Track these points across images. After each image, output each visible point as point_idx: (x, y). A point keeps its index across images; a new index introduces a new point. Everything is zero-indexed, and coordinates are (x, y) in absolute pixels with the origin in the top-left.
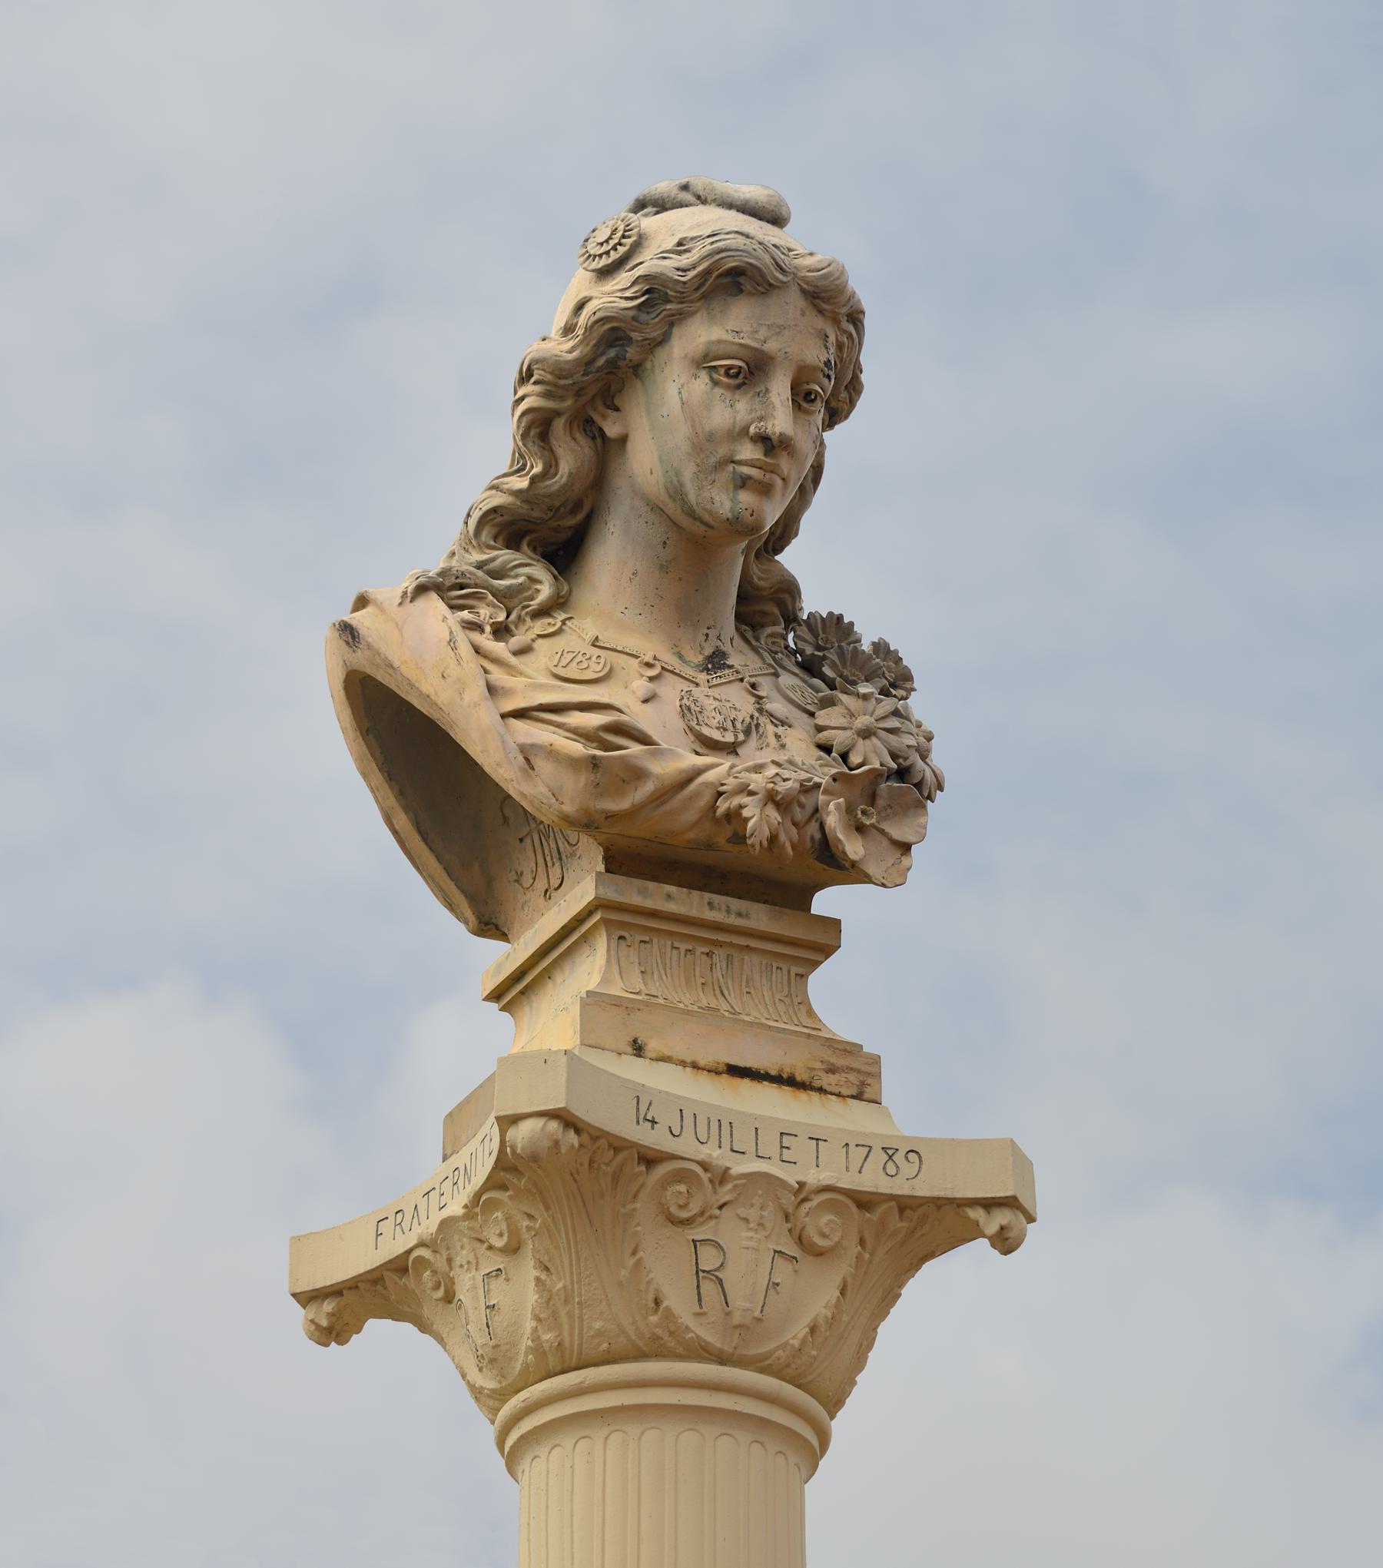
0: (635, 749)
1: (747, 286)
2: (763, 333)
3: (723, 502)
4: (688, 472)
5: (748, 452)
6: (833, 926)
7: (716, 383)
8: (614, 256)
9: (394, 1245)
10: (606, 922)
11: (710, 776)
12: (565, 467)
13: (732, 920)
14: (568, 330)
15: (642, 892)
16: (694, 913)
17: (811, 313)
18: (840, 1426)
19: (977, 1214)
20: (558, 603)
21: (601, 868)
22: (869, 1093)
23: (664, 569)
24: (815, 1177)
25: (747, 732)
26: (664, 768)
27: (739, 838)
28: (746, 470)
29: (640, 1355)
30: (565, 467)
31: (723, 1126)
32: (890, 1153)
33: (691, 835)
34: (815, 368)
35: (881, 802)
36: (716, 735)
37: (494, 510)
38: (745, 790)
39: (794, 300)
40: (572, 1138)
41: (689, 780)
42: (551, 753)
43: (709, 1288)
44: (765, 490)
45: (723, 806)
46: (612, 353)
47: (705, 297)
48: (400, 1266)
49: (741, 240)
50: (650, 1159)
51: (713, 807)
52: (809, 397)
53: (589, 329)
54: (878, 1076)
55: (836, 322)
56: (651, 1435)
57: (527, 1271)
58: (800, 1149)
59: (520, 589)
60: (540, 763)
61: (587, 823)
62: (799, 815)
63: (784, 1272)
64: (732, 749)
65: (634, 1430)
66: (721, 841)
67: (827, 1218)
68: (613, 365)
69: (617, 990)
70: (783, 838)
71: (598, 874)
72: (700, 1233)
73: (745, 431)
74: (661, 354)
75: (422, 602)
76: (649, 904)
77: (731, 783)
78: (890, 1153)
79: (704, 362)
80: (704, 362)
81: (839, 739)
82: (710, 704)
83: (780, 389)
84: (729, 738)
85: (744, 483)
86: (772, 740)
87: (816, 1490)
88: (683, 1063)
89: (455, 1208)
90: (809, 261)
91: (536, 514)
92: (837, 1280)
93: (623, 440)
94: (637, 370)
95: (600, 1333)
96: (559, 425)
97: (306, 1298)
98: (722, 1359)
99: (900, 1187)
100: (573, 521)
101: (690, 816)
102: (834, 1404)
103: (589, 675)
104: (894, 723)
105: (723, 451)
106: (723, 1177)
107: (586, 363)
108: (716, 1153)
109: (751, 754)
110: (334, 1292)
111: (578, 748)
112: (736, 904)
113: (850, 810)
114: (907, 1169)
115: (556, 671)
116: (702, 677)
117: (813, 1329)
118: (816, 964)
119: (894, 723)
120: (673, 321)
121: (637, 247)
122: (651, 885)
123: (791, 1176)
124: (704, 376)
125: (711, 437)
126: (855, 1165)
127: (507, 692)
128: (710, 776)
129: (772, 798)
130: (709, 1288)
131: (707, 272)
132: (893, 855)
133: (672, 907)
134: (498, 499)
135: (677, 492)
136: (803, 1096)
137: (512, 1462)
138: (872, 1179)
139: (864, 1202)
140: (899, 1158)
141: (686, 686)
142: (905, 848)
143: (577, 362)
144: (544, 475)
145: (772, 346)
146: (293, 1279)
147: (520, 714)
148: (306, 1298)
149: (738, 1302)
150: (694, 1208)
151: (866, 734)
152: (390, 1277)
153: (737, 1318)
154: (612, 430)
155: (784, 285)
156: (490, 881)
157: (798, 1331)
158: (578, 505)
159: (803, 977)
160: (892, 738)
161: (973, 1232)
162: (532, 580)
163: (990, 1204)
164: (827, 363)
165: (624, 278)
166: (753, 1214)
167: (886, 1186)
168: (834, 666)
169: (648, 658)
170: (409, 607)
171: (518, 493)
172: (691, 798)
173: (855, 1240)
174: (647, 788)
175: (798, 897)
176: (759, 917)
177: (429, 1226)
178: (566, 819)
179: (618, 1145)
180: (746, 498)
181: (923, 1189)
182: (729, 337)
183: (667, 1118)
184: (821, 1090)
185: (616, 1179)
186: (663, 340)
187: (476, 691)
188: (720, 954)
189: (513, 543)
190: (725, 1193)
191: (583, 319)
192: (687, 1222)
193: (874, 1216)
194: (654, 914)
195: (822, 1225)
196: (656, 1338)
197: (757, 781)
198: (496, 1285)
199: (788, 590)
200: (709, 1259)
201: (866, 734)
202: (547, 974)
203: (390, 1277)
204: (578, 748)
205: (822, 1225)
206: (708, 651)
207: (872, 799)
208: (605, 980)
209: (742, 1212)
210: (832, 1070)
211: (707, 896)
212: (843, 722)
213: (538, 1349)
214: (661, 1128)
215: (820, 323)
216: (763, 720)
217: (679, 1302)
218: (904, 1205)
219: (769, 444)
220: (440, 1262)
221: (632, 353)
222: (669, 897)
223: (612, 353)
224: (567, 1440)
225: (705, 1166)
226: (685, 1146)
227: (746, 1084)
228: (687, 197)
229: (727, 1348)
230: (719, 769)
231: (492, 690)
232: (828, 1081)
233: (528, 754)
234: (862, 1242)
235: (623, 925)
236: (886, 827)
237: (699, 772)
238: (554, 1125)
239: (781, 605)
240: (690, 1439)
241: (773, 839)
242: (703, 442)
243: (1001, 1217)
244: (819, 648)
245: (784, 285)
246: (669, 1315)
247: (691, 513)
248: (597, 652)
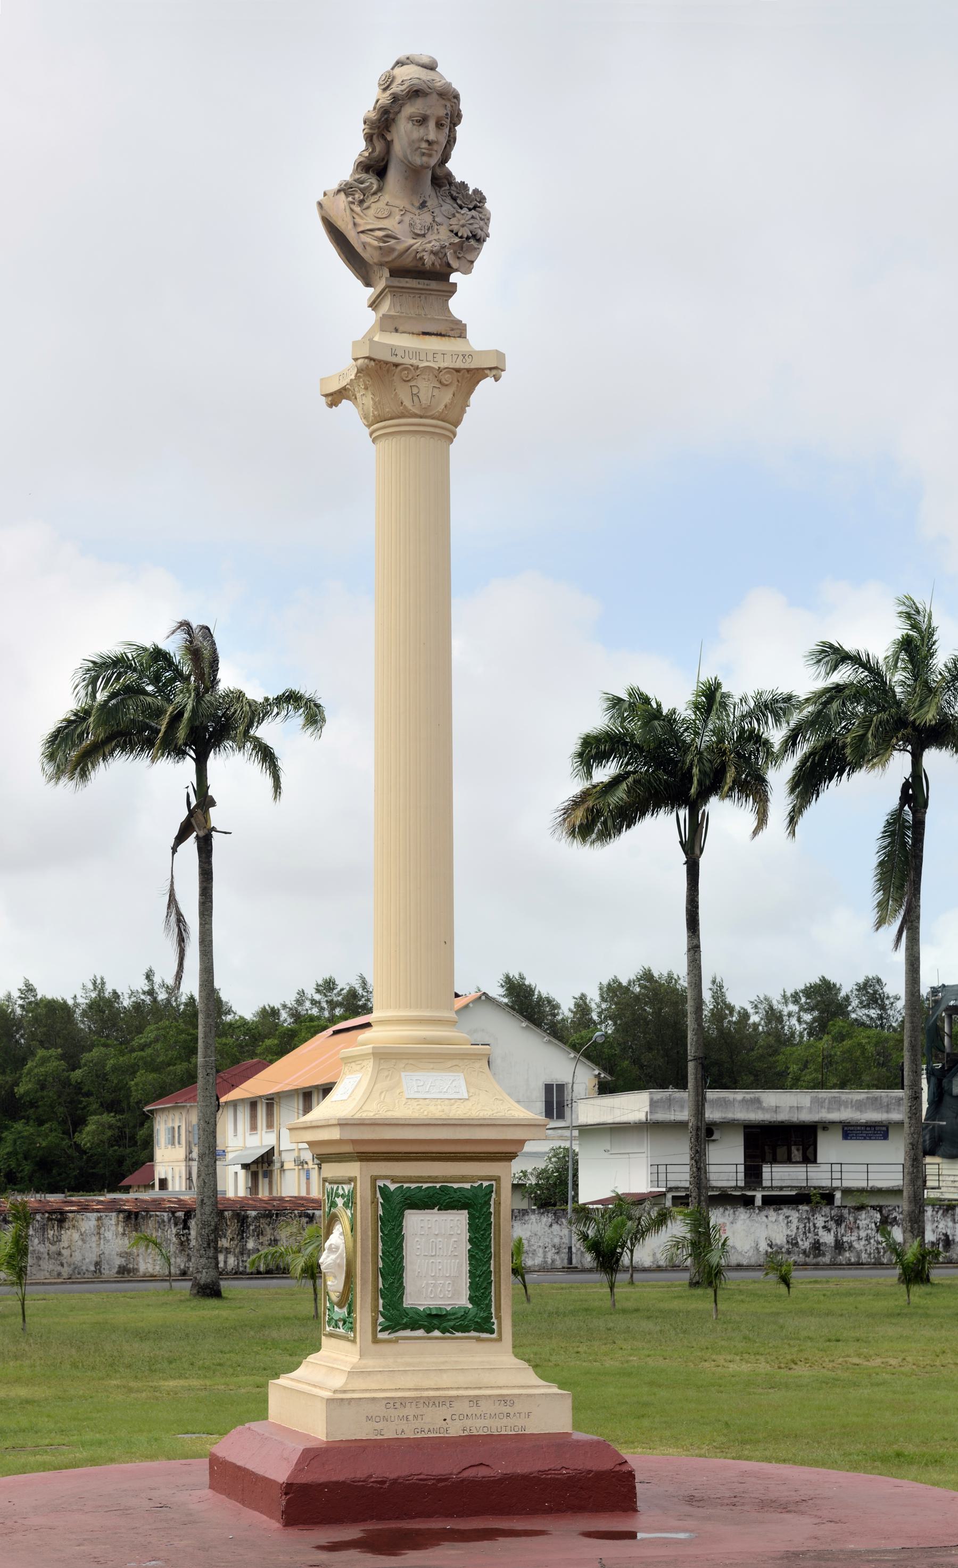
0: (393, 241)
1: (420, 94)
2: (426, 108)
3: (418, 160)
4: (408, 152)
5: (424, 145)
6: (455, 285)
7: (414, 125)
8: (386, 85)
9: (343, 383)
10: (390, 291)
11: (414, 247)
12: (378, 149)
13: (425, 287)
14: (375, 108)
15: (399, 282)
16: (414, 286)
17: (441, 99)
18: (459, 430)
19: (487, 372)
20: (380, 189)
21: (388, 275)
22: (463, 335)
23: (406, 179)
24: (443, 365)
25: (428, 230)
26: (400, 247)
27: (423, 264)
28: (424, 151)
29: (399, 417)
30: (378, 149)
31: (417, 353)
32: (464, 356)
33: (411, 264)
34: (442, 117)
35: (464, 249)
36: (419, 232)
37: (361, 162)
38: (424, 250)
39: (435, 96)
40: (373, 363)
41: (409, 249)
42: (370, 244)
43: (415, 398)
44: (430, 156)
45: (418, 256)
46: (386, 116)
47: (409, 98)
48: (344, 389)
49: (418, 80)
50: (396, 365)
51: (416, 256)
52: (442, 125)
53: (379, 110)
54: (465, 330)
55: (449, 100)
56: (403, 438)
57: (370, 396)
58: (439, 357)
59: (368, 187)
60: (367, 247)
61: (381, 264)
62: (441, 255)
63: (436, 392)
64: (424, 236)
65: (399, 437)
66: (420, 265)
67: (448, 375)
68: (387, 120)
69: (392, 313)
70: (436, 263)
71: (386, 278)
72: (412, 383)
73: (422, 139)
74: (399, 115)
75: (339, 196)
76: (401, 285)
77: (421, 248)
78: (464, 356)
79: (410, 118)
80: (410, 118)
81: (455, 228)
82: (418, 221)
83: (432, 124)
84: (423, 232)
85: (423, 154)
86: (435, 231)
87: (451, 446)
88: (409, 333)
89: (353, 377)
90: (439, 84)
91: (372, 163)
92: (452, 392)
93: (392, 141)
94: (393, 120)
95: (388, 412)
96: (375, 137)
97: (326, 396)
98: (421, 417)
99: (467, 366)
100: (382, 164)
101: (410, 259)
102: (456, 423)
103: (384, 216)
104: (472, 221)
105: (417, 145)
106: (417, 368)
107: (380, 120)
108: (415, 361)
109: (430, 237)
110: (331, 394)
111: (376, 243)
112: (426, 282)
113: (455, 252)
114: (469, 360)
115: (376, 215)
116: (417, 212)
117: (446, 406)
118: (451, 296)
119: (472, 221)
120: (401, 106)
121: (392, 82)
122: (401, 279)
123: (436, 366)
124: (410, 122)
125: (413, 141)
126: (454, 361)
127: (359, 225)
128: (414, 247)
129: (432, 252)
130: (415, 398)
131: (409, 91)
132: (468, 264)
133: (408, 285)
134: (362, 159)
135: (405, 157)
136: (443, 338)
137: (374, 441)
138: (459, 364)
139: (458, 370)
140: (466, 357)
141: (412, 216)
142: (472, 262)
143: (376, 120)
144: (372, 152)
145: (428, 113)
146: (321, 390)
147: (362, 232)
148: (326, 396)
149: (423, 402)
150: (410, 377)
151: (463, 226)
152: (343, 392)
153: (423, 406)
154: (389, 138)
155: (431, 93)
156: (367, 273)
157: (442, 407)
158: (383, 159)
159: (447, 301)
160: (470, 226)
161: (487, 376)
162: (371, 183)
163: (491, 369)
164: (447, 114)
165: (389, 92)
166: (426, 377)
167: (462, 366)
168: (461, 199)
169: (401, 208)
170: (336, 197)
171: (366, 157)
172: (409, 254)
173: (456, 380)
174: (396, 254)
175: (446, 277)
176: (434, 285)
177: (348, 381)
178: (375, 263)
179: (387, 363)
180: (425, 159)
181: (472, 366)
182: (416, 111)
183: (400, 353)
184: (449, 336)
185: (388, 371)
186: (399, 112)
187: (351, 225)
188: (423, 297)
189: (367, 171)
190: (418, 372)
191: (378, 106)
192: (408, 381)
193: (461, 374)
194: (403, 288)
195: (446, 378)
196: (402, 413)
197: (429, 246)
198: (364, 398)
199: (449, 176)
200: (415, 391)
201: (463, 226)
202: (380, 302)
203: (343, 392)
204: (376, 243)
205: (446, 378)
206: (421, 202)
207: (462, 249)
208: (389, 309)
209: (423, 377)
210: (452, 330)
211: (418, 280)
212: (457, 223)
213: (374, 416)
214: (399, 356)
215: (443, 102)
216: (434, 224)
217: (408, 403)
218: (468, 370)
219: (430, 143)
220: (352, 389)
221: (391, 116)
222: (407, 282)
223: (386, 116)
224: (383, 440)
225: (412, 366)
226: (406, 361)
227: (427, 337)
228: (408, 61)
229: (422, 414)
230: (418, 244)
231: (355, 224)
232: (451, 333)
233: (364, 245)
234: (458, 381)
235: (394, 292)
236: (466, 256)
237: (412, 246)
238: (366, 361)
239: (448, 180)
240: (413, 439)
241: (433, 264)
242: (412, 142)
243: (494, 372)
244: (458, 193)
245: (431, 93)
246: (405, 407)
247: (410, 163)
248: (387, 207)
